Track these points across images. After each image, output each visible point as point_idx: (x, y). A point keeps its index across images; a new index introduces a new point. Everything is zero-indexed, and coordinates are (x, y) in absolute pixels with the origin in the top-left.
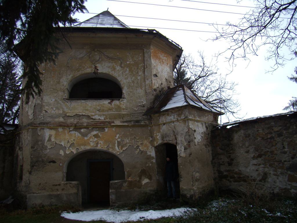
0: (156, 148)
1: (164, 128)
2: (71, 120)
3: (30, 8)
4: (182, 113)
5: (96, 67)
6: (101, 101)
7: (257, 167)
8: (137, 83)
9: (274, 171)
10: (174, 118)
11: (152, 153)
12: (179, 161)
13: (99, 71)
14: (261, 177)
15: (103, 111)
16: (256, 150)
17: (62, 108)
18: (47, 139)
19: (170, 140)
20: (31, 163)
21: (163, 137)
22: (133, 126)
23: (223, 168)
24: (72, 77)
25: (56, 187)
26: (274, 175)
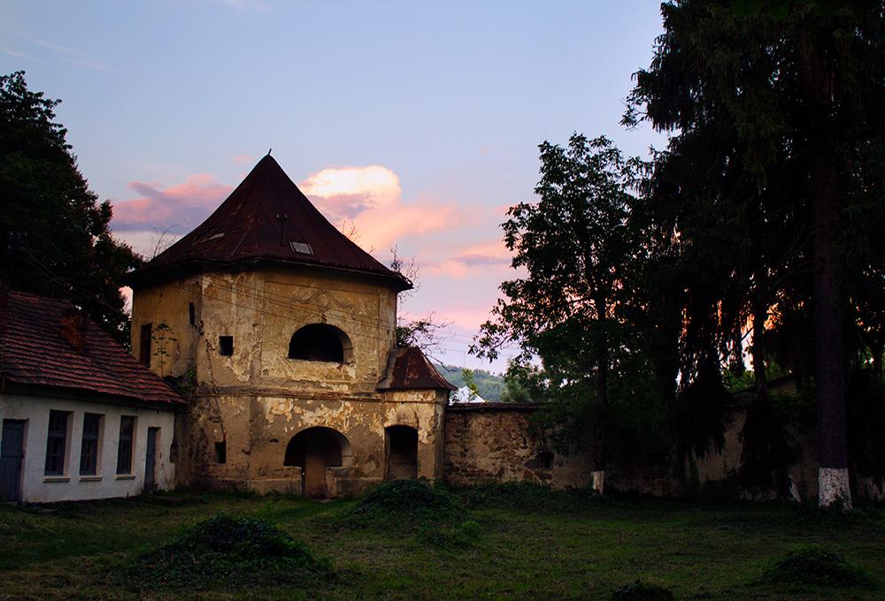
0: (387, 429)
1: (401, 407)
2: (295, 389)
3: (682, 339)
4: (429, 394)
5: (324, 317)
6: (329, 364)
7: (493, 461)
8: (370, 343)
9: (511, 466)
10: (418, 398)
11: (381, 433)
12: (420, 447)
13: (327, 323)
14: (497, 472)
15: (331, 378)
16: (496, 441)
17: (286, 371)
18: (268, 411)
19: (410, 422)
20: (251, 441)
21: (399, 418)
22: (364, 400)
23: (453, 459)
24: (296, 327)
25: (278, 473)
26: (511, 470)
